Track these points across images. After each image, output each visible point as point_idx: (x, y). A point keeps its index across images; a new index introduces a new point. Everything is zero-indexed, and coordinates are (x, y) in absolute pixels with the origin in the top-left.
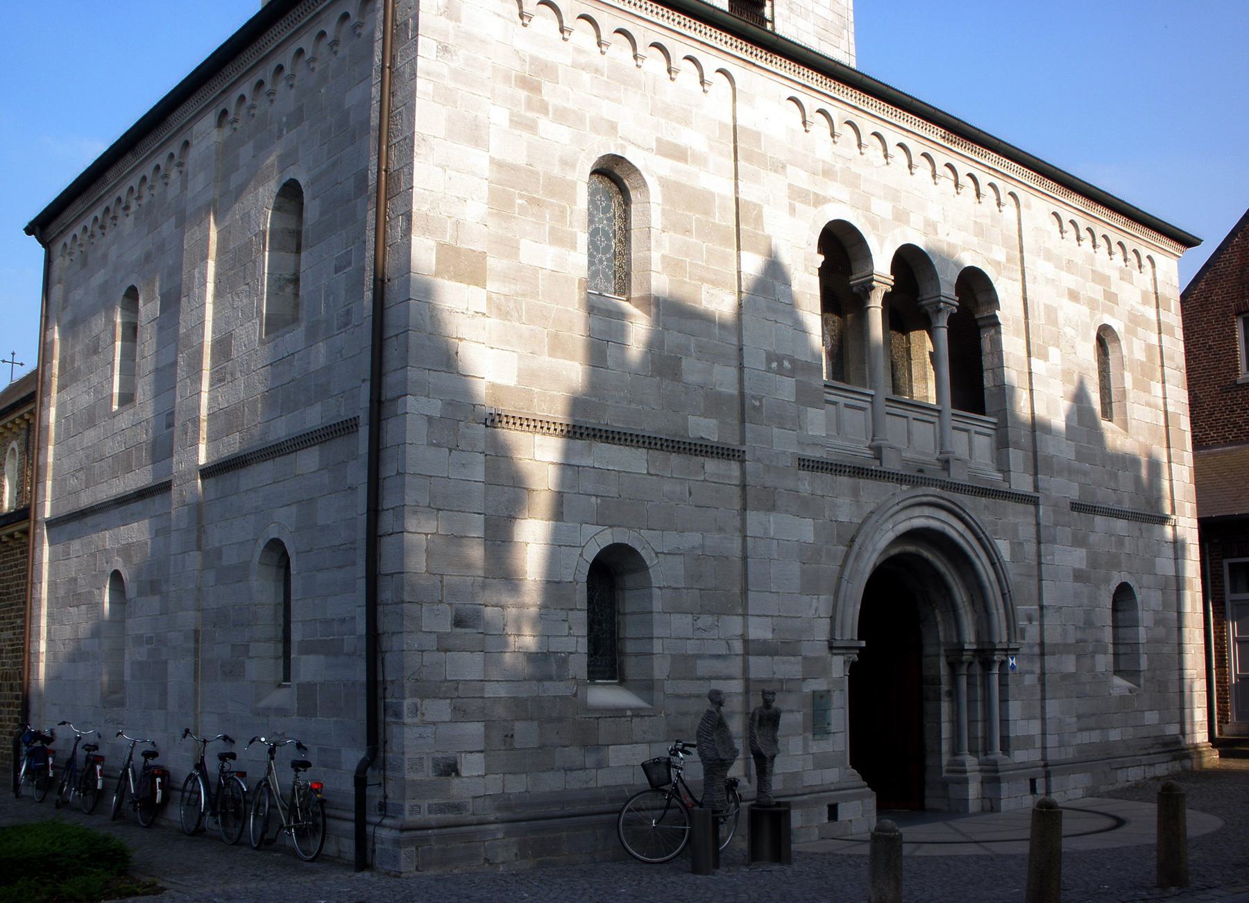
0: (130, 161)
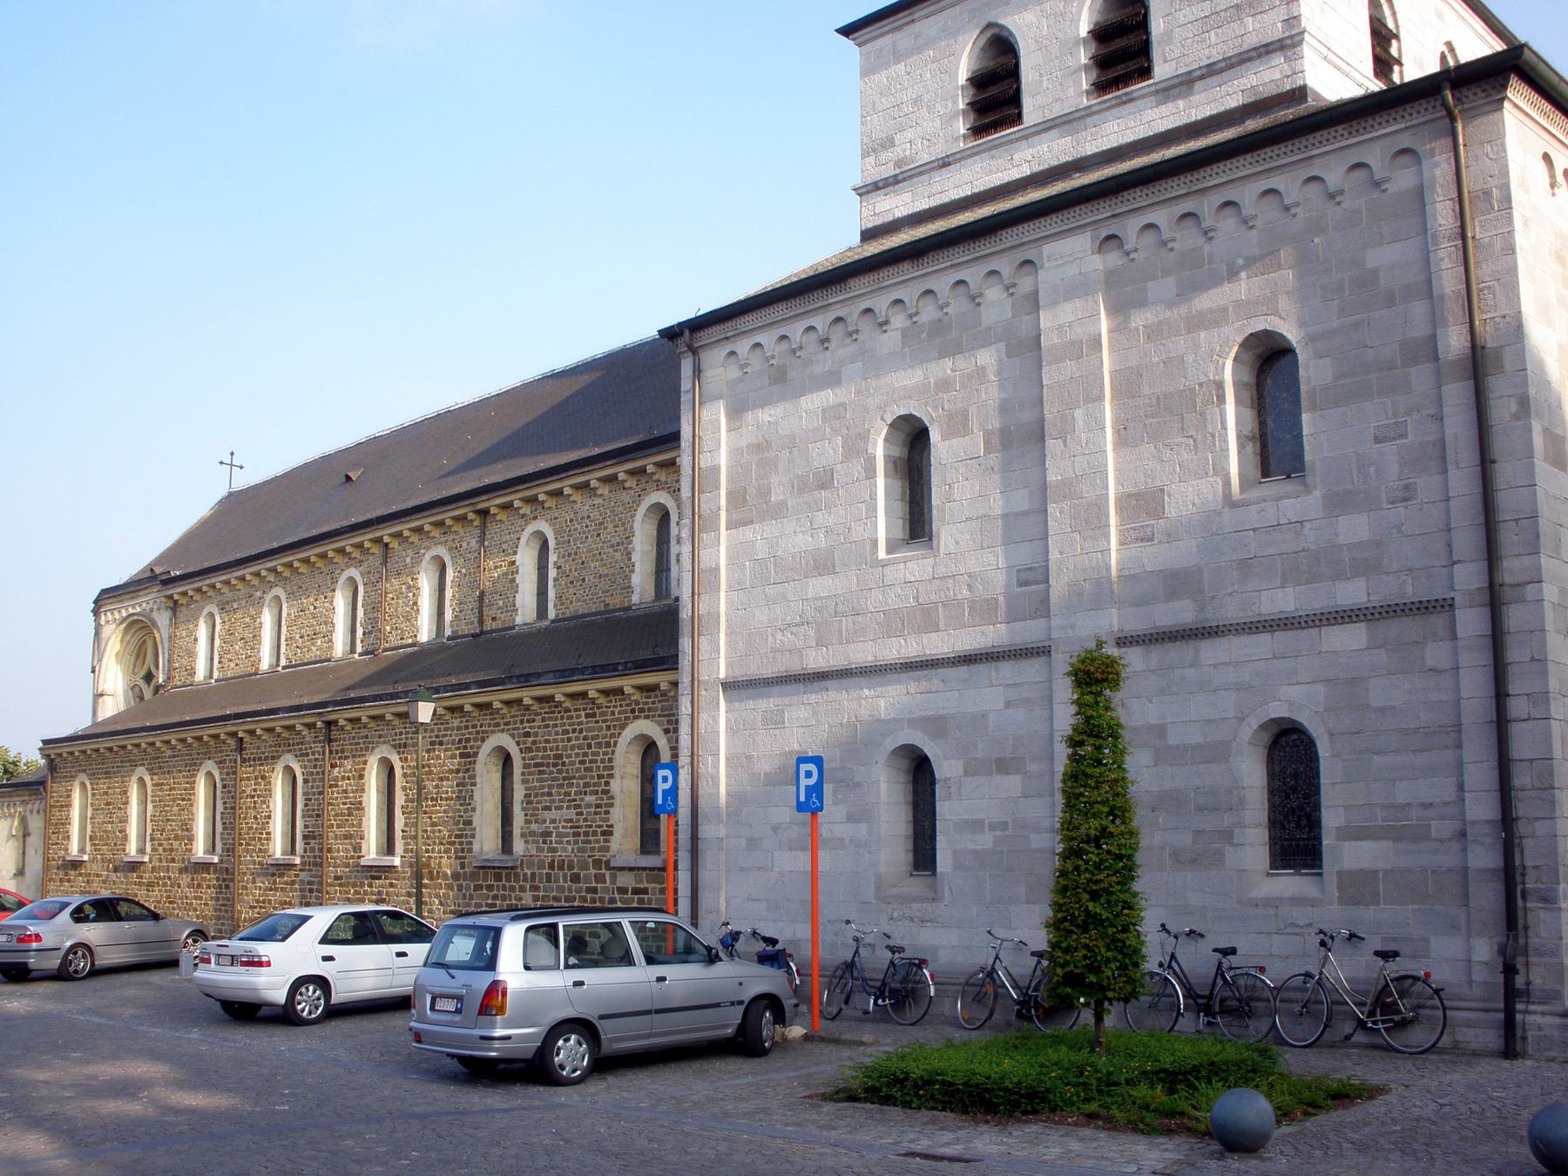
0: (906, 270)
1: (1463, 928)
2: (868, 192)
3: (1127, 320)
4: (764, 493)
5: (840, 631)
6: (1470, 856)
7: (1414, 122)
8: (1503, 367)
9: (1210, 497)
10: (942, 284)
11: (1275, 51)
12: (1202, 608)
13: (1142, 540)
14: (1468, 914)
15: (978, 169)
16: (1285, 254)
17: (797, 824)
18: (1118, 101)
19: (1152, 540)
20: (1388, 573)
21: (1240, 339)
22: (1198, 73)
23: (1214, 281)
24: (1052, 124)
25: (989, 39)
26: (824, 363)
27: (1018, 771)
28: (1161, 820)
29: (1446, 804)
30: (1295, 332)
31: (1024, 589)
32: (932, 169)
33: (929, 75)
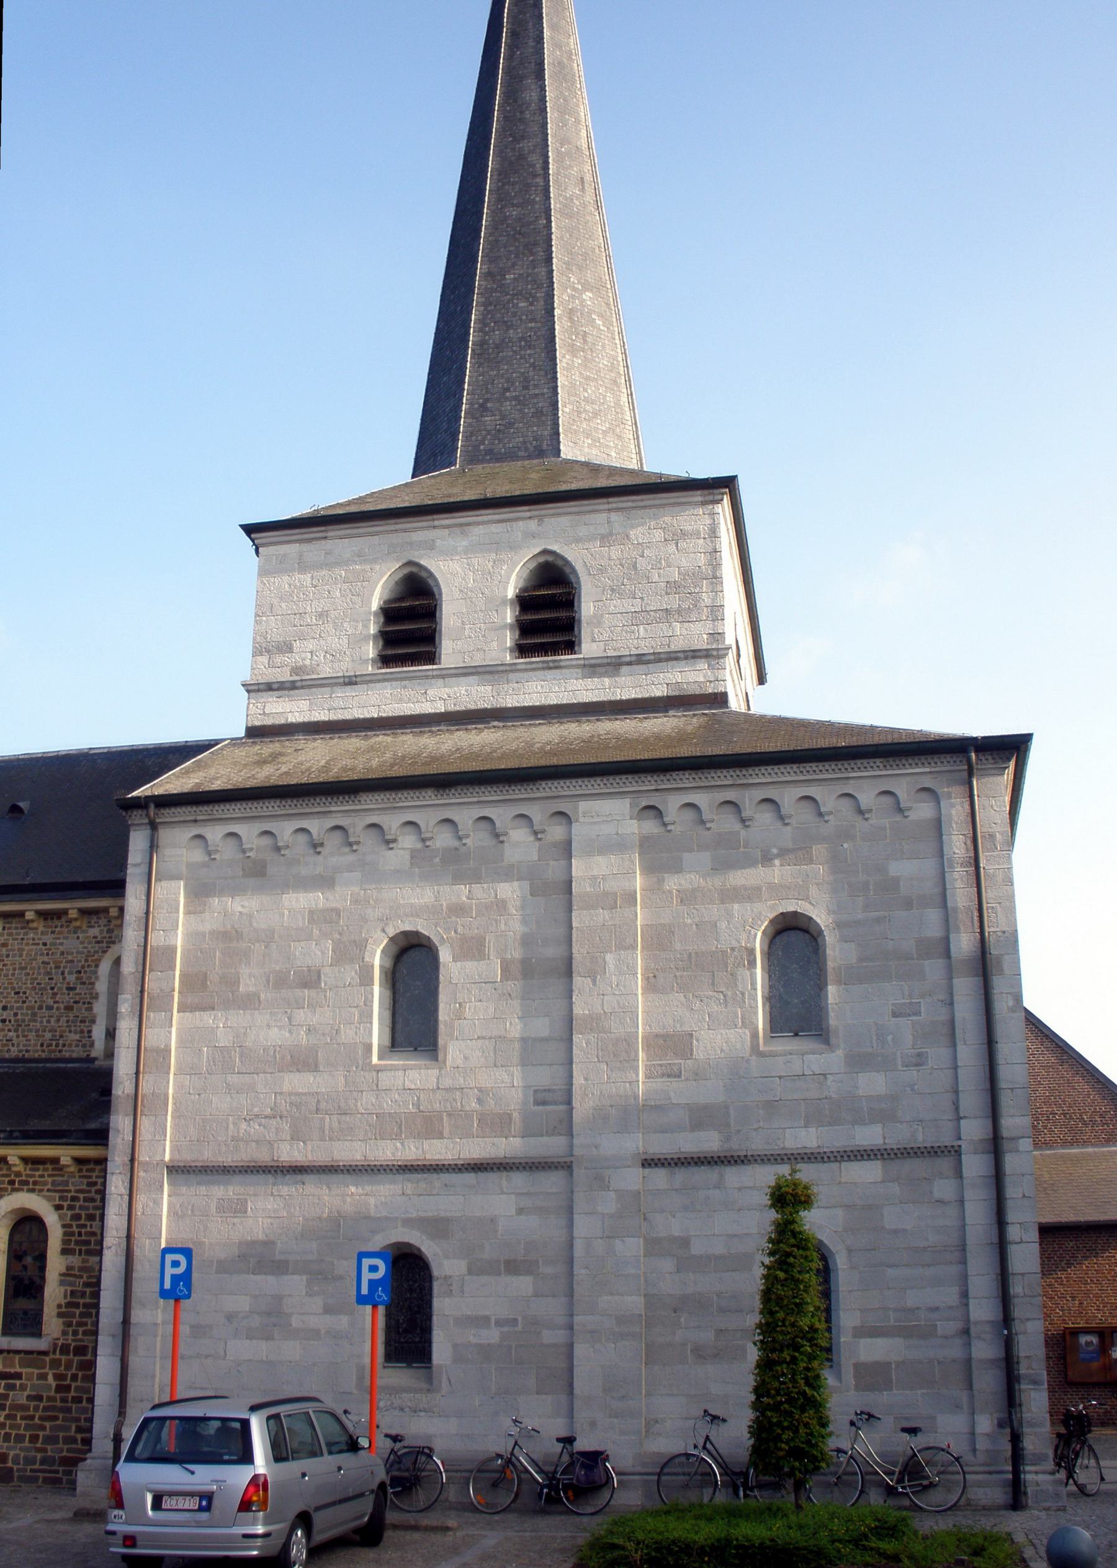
0: (429, 796)
1: (965, 1407)
2: (259, 691)
3: (661, 881)
4: (231, 982)
5: (322, 1129)
6: (973, 1349)
7: (937, 769)
8: (1002, 970)
9: (739, 1046)
10: (465, 817)
11: (700, 657)
12: (728, 1139)
13: (669, 1076)
14: (971, 1397)
15: (388, 696)
16: (819, 850)
17: (258, 1313)
18: (545, 665)
19: (680, 1076)
20: (902, 1122)
21: (772, 916)
22: (628, 659)
23: (749, 862)
24: (474, 670)
25: (405, 575)
26: (316, 865)
27: (529, 1272)
28: (682, 1320)
29: (950, 1308)
30: (823, 917)
31: (541, 1108)
32: (336, 684)
33: (338, 594)
